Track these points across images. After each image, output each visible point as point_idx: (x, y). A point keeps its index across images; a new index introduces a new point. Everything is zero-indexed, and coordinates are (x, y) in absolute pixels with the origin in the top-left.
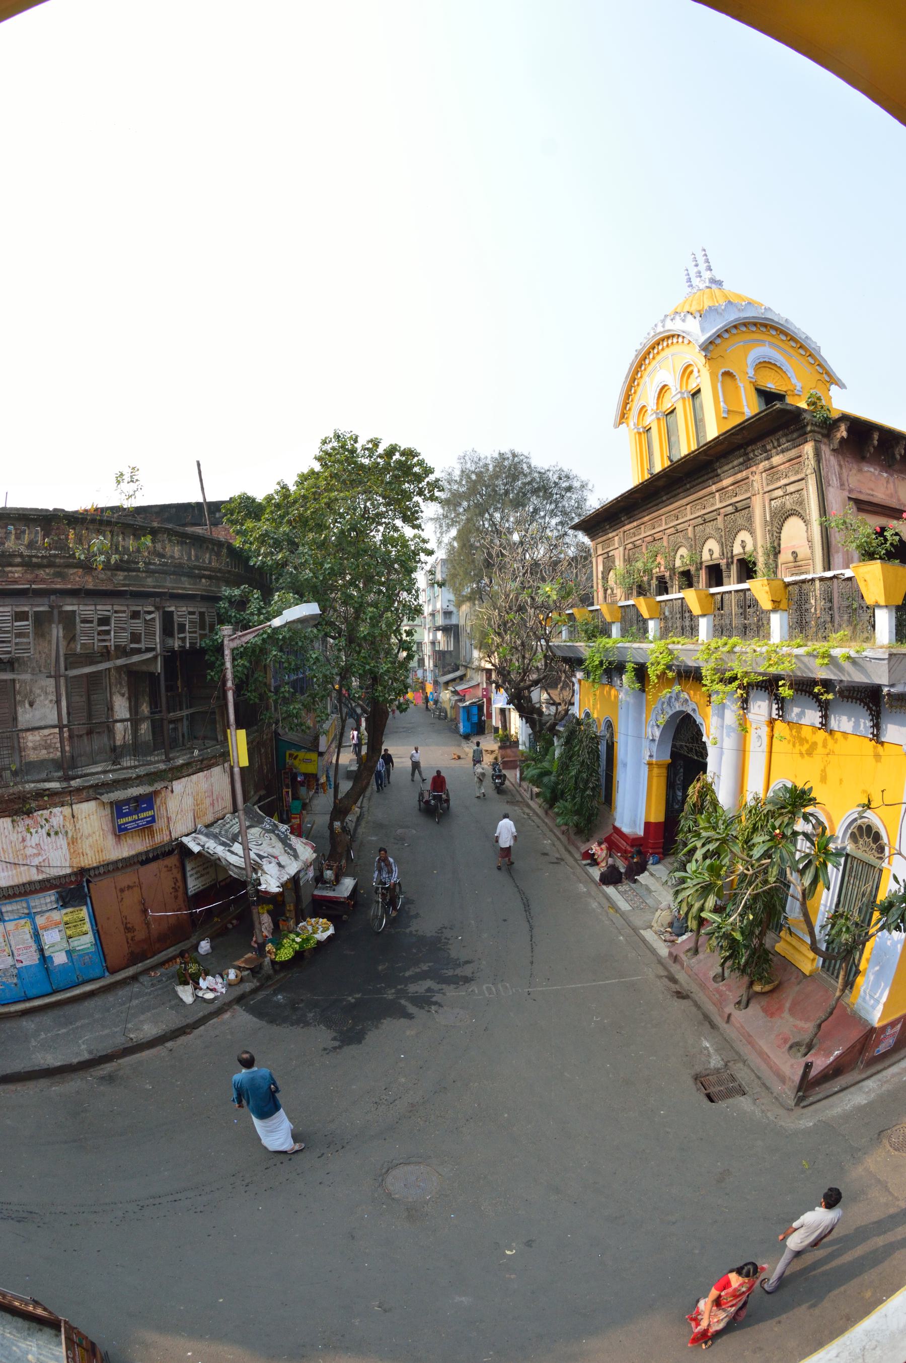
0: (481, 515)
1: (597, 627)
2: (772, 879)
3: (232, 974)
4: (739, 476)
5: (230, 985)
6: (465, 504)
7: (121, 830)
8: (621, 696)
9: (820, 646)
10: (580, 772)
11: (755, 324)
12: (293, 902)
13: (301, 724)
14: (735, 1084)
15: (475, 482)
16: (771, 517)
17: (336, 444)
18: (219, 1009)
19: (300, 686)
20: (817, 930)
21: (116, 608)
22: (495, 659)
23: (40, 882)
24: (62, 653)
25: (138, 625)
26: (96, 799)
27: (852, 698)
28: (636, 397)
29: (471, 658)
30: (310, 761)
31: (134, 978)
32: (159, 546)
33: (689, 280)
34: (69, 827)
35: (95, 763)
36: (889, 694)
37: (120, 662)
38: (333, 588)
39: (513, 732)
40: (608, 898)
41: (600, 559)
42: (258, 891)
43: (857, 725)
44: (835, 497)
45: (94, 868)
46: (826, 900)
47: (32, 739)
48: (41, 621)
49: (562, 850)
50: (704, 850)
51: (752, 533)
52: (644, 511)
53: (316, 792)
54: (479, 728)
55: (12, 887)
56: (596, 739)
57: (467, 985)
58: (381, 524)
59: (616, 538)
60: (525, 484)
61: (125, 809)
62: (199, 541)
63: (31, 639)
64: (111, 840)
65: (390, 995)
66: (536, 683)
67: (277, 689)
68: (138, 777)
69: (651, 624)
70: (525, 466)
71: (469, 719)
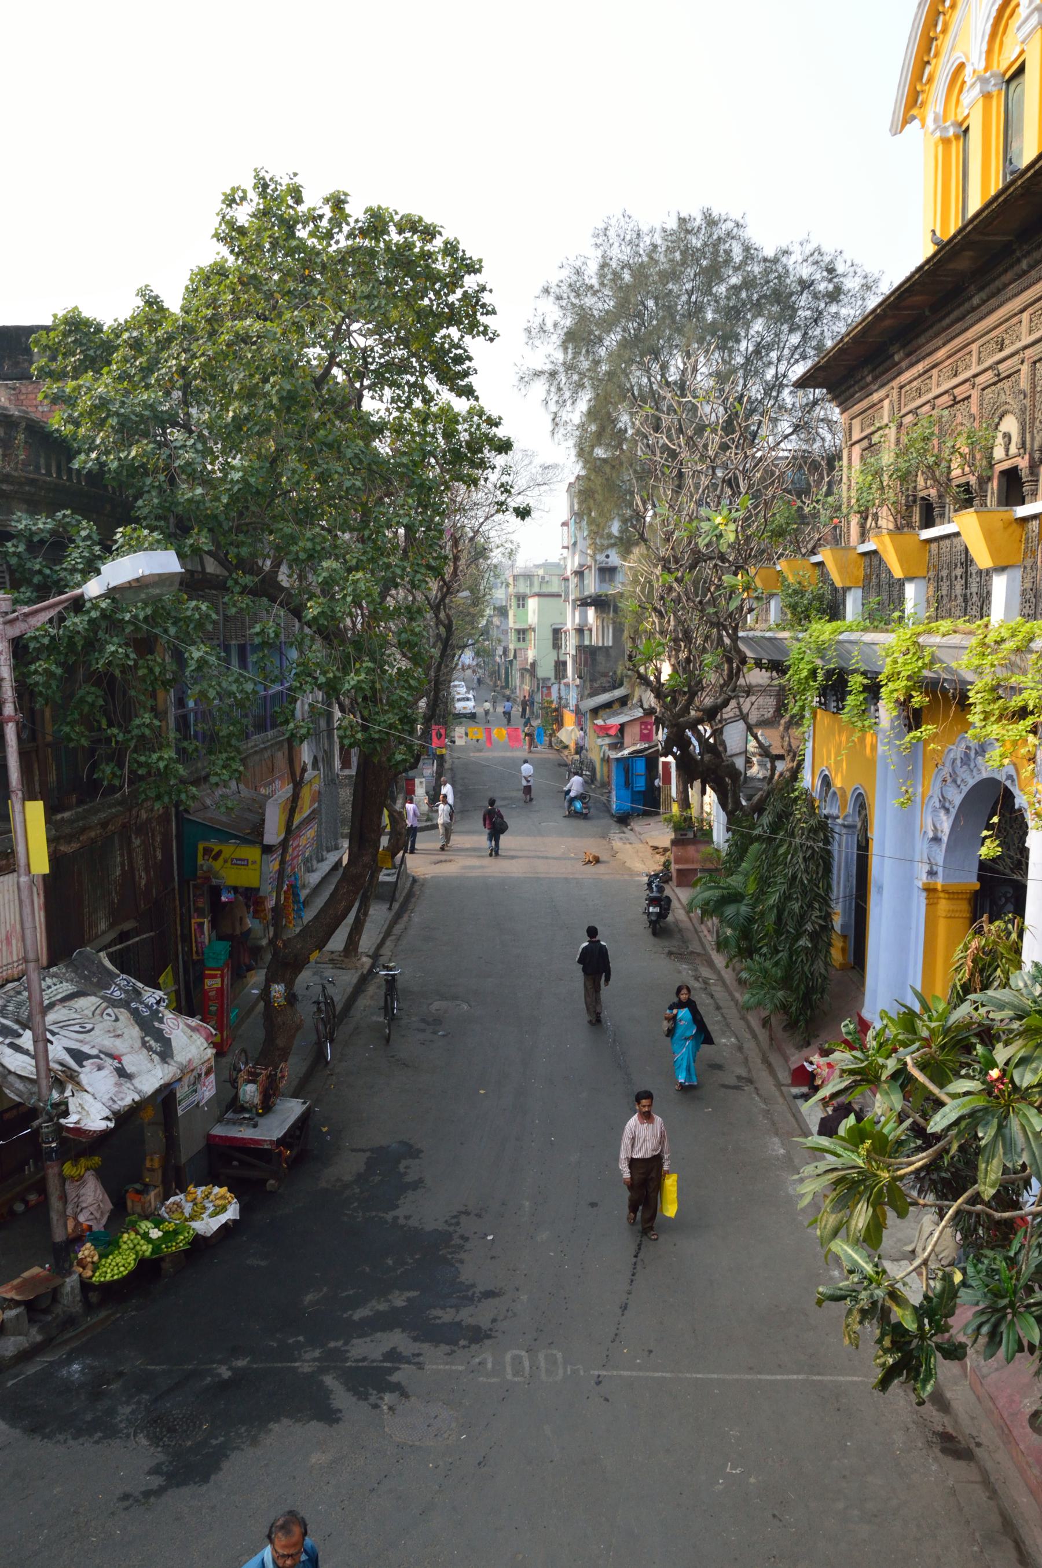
10: (787, 897)
12: (144, 1147)
30: (243, 862)
41: (857, 450)
42: (62, 1128)
52: (937, 335)
57: (474, 1347)
59: (886, 402)
71: (628, 783)
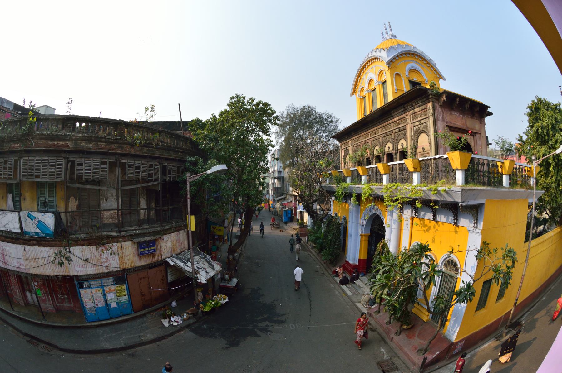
0: (295, 131)
1: (341, 178)
2: (412, 282)
3: (185, 316)
4: (401, 117)
5: (184, 320)
6: (288, 127)
7: (141, 254)
8: (350, 207)
9: (433, 186)
11: (409, 54)
12: (213, 287)
13: (218, 215)
14: (394, 366)
15: (293, 118)
16: (414, 133)
17: (236, 100)
18: (179, 329)
19: (218, 199)
20: (430, 303)
21: (143, 162)
22: (299, 191)
23: (107, 273)
24: (120, 179)
25: (152, 170)
26: (131, 241)
27: (446, 208)
28: (360, 84)
29: (289, 190)
31: (144, 315)
32: (161, 138)
33: (383, 35)
34: (120, 252)
35: (131, 226)
36: (461, 206)
37: (144, 185)
38: (233, 159)
39: (305, 221)
40: (343, 290)
41: (343, 151)
43: (448, 219)
44: (440, 125)
45: (129, 269)
46: (434, 290)
47: (106, 214)
48: (112, 166)
49: (324, 270)
50: (383, 270)
51: (406, 140)
53: (223, 243)
54: (291, 219)
55: (95, 274)
56: (339, 225)
58: (253, 133)
60: (313, 119)
61: (143, 245)
62: (178, 137)
63: (107, 173)
64: (137, 258)
65: (250, 327)
66: (315, 201)
67: (208, 199)
68: (149, 233)
69: (363, 178)
70: (313, 112)
71: (287, 215)
